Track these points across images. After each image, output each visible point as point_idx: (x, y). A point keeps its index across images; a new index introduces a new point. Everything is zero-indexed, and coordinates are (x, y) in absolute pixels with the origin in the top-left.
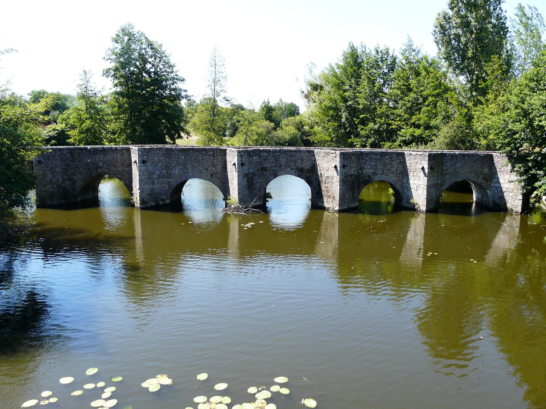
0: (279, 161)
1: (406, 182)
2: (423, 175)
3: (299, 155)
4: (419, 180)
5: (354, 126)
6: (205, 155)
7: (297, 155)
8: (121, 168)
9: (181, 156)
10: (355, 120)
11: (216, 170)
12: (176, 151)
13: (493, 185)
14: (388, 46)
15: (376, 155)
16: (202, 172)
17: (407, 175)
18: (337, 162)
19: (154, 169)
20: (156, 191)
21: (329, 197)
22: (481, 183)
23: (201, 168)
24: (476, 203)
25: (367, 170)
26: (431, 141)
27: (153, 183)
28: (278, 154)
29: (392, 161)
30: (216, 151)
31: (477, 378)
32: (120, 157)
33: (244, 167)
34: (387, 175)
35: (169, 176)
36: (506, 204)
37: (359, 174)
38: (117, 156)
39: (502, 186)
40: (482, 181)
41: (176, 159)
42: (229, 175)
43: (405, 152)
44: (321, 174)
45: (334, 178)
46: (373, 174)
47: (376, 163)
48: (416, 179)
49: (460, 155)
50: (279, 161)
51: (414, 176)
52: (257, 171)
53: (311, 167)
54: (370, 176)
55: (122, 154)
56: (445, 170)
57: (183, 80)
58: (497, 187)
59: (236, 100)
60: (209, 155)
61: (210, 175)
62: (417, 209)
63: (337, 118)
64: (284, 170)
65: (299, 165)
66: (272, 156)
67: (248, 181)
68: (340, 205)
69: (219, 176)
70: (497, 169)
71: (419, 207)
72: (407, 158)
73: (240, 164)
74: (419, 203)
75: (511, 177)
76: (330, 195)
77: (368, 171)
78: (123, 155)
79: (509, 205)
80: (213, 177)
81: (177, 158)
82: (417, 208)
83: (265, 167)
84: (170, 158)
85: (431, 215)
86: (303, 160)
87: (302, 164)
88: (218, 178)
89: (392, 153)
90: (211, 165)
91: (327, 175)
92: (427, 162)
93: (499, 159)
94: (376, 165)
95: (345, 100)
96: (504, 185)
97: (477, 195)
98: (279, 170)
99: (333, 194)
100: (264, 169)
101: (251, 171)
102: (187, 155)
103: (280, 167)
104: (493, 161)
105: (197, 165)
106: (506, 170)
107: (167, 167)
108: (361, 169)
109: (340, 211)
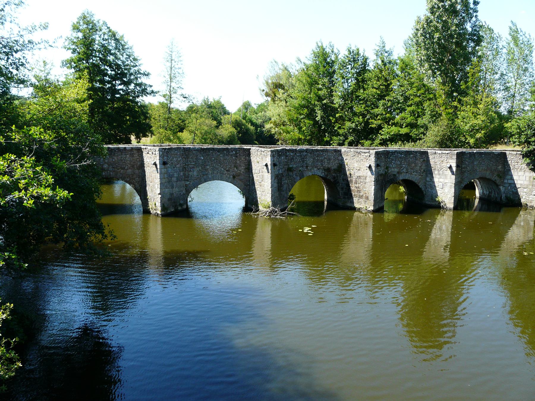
0: (306, 161)
1: (429, 180)
2: (450, 174)
3: (326, 155)
4: (446, 178)
5: (330, 125)
6: (227, 155)
7: (324, 154)
8: (130, 170)
9: (201, 157)
10: (331, 118)
11: (239, 171)
12: (195, 150)
13: (506, 181)
14: (358, 47)
15: (401, 154)
16: (223, 174)
17: (431, 174)
18: (372, 161)
19: (173, 172)
20: (175, 195)
21: (361, 197)
22: (496, 180)
23: (223, 169)
24: (480, 198)
25: (393, 170)
26: (420, 139)
27: (172, 187)
28: (305, 153)
29: (416, 159)
30: (239, 151)
31: (424, 360)
32: (129, 158)
33: (276, 167)
34: (411, 174)
35: (186, 179)
36: (520, 199)
37: (386, 173)
38: (126, 157)
39: (516, 183)
40: (497, 178)
41: (195, 160)
42: (255, 176)
43: (428, 151)
44: (350, 174)
45: (368, 178)
46: (398, 173)
47: (401, 162)
48: (442, 177)
49: (478, 154)
50: (306, 161)
51: (439, 174)
52: (284, 171)
53: (338, 167)
54: (394, 175)
55: (132, 155)
56: (464, 168)
57: (147, 75)
58: (510, 184)
59: (193, 97)
60: (232, 155)
61: (232, 177)
62: (443, 207)
63: (311, 115)
64: (311, 170)
65: (326, 165)
66: (298, 156)
67: (278, 183)
68: (374, 206)
69: (242, 177)
70: (511, 166)
71: (445, 205)
72: (431, 157)
73: (273, 165)
74: (445, 201)
75: (526, 174)
76: (362, 196)
77: (394, 170)
78: (133, 156)
79: (524, 201)
80: (235, 179)
81: (196, 159)
82: (443, 206)
83: (291, 168)
84: (188, 158)
85: (455, 211)
86: (329, 159)
87: (329, 163)
88: (241, 180)
89: (416, 152)
90: (233, 166)
91: (358, 175)
92: (455, 161)
93: (512, 157)
94: (401, 164)
95: (320, 99)
96: (518, 181)
97: (481, 191)
98: (305, 171)
99: (366, 194)
100: (290, 170)
101: (281, 172)
102: (207, 155)
103: (307, 167)
104: (507, 158)
105: (218, 165)
106: (520, 167)
107: (184, 169)
108: (387, 168)
109: (374, 212)
